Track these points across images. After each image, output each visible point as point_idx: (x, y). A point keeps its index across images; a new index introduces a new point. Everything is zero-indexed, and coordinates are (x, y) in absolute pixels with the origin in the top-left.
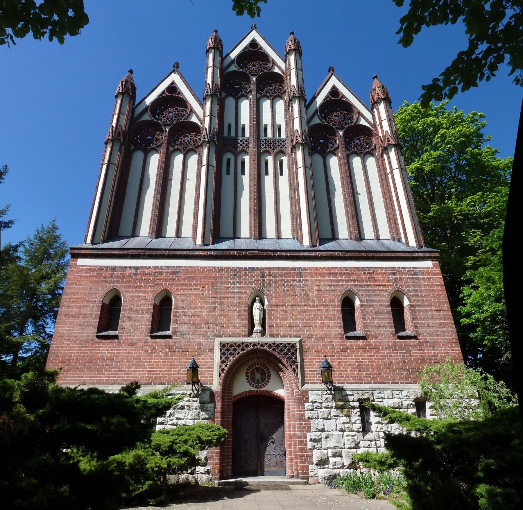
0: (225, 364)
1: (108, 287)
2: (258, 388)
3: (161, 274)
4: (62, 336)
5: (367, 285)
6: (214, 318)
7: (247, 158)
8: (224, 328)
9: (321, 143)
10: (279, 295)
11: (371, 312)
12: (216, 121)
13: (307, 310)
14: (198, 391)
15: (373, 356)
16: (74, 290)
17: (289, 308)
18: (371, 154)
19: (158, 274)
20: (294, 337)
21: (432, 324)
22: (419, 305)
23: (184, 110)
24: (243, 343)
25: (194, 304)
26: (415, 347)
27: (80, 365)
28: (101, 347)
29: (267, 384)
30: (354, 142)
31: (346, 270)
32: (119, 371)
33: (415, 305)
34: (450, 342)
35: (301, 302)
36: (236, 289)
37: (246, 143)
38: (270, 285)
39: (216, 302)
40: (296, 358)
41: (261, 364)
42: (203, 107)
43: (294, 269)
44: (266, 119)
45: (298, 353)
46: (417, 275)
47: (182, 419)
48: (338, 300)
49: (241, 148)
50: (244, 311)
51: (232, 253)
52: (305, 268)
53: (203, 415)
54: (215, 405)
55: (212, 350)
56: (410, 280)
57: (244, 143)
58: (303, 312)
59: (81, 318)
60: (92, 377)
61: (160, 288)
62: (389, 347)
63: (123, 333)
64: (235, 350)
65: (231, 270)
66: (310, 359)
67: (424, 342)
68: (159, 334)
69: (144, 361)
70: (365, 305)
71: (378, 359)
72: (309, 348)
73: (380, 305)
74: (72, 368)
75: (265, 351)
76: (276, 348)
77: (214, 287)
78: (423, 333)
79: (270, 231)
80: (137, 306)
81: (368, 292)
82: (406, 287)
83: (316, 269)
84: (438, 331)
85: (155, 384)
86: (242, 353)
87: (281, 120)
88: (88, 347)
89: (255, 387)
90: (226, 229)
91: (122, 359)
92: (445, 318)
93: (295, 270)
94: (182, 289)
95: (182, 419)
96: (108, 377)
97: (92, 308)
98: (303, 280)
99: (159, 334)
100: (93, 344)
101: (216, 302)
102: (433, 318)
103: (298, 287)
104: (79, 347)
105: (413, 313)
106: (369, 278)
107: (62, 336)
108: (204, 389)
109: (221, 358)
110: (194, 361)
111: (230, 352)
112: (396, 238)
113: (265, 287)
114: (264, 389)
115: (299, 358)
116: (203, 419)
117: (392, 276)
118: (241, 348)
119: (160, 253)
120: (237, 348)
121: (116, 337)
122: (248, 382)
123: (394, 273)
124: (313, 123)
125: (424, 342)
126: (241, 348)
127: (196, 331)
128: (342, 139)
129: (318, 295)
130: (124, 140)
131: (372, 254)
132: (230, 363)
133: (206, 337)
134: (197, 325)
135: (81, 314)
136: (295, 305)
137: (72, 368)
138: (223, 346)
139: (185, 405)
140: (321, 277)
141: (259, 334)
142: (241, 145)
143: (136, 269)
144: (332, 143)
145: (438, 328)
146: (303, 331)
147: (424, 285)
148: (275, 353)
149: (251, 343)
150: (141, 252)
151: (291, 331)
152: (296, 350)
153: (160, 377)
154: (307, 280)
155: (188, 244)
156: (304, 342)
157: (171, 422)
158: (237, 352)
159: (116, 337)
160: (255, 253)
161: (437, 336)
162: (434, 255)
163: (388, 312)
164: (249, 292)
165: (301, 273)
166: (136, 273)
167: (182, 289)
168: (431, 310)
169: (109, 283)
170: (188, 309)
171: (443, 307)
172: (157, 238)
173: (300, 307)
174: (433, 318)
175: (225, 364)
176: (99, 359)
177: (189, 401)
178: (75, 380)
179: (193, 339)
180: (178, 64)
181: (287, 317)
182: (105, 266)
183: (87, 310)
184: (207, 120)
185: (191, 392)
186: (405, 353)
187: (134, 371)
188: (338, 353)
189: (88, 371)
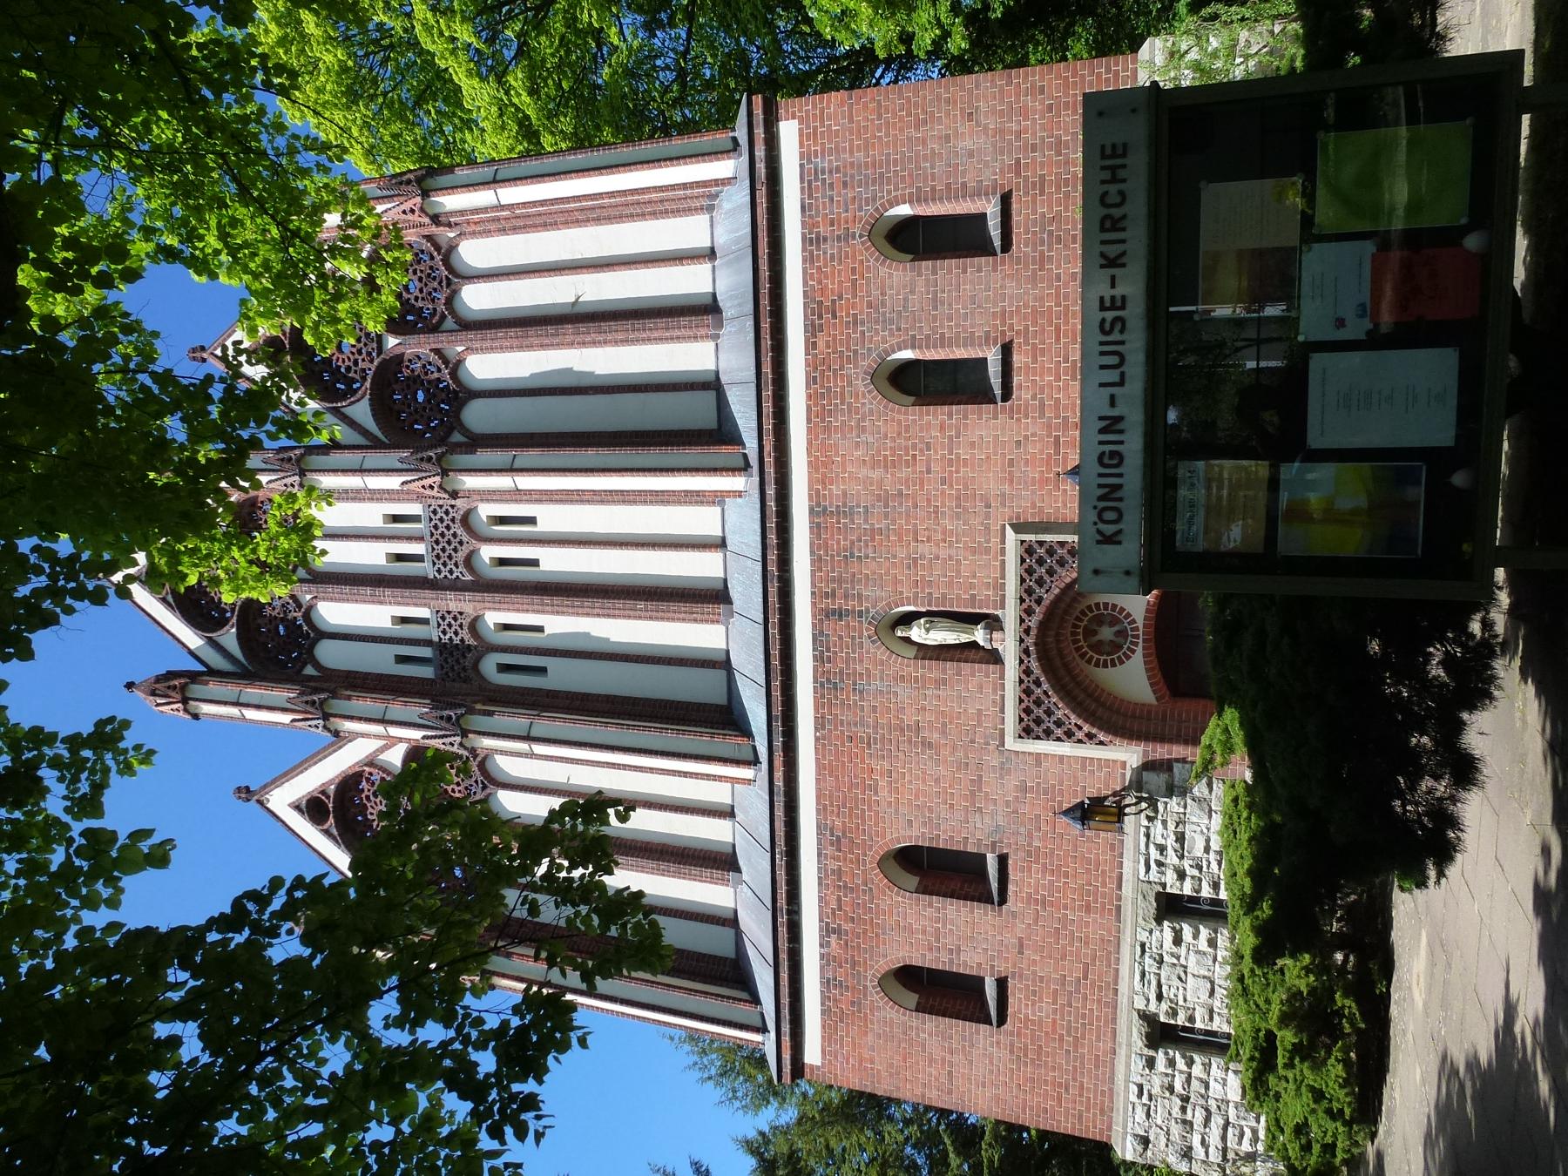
0: (1074, 729)
1: (875, 996)
2: (1137, 637)
3: (839, 873)
4: (997, 1099)
5: (855, 323)
6: (954, 748)
7: (493, 618)
8: (980, 723)
9: (427, 400)
10: (888, 574)
11: (935, 320)
12: (397, 709)
13: (929, 501)
14: (1140, 800)
15: (1058, 329)
16: (884, 1074)
17: (924, 549)
18: (448, 253)
19: (840, 879)
20: (1003, 542)
21: (967, 144)
22: (910, 175)
23: (368, 780)
24: (1021, 681)
25: (917, 796)
26: (1034, 202)
27: (1068, 1063)
28: (1026, 1016)
29: (1129, 615)
30: (416, 299)
31: (815, 383)
32: (1086, 978)
33: (911, 186)
34: (1018, 95)
35: (908, 515)
36: (873, 687)
37: (449, 619)
38: (860, 596)
39: (910, 741)
40: (1062, 544)
41: (1075, 626)
42: (355, 736)
43: (816, 529)
44: (372, 556)
45: (1048, 538)
46: (823, 173)
47: (1208, 841)
48: (899, 412)
49: (465, 634)
50: (934, 670)
51: (777, 694)
52: (810, 496)
53: (1200, 789)
54: (1177, 760)
55: (1038, 757)
56: (839, 195)
57: (450, 625)
58: (936, 512)
59: (955, 1059)
60: (1098, 1038)
61: (877, 876)
62: (1034, 279)
63: (992, 967)
64: (1038, 703)
65: (823, 696)
66: (1065, 506)
67: (1018, 174)
68: (994, 885)
69: (1064, 920)
70: (914, 337)
71: (1066, 315)
72: (1034, 506)
73: (912, 292)
74: (1075, 1080)
75: (1043, 626)
76: (1035, 596)
77: (869, 744)
78: (993, 172)
79: (690, 281)
80: (924, 932)
81: (877, 322)
82: (861, 209)
83: (813, 465)
84: (986, 128)
85: (1119, 898)
86: (1045, 686)
87: (371, 515)
88: (1026, 1046)
89: (1136, 644)
90: (695, 411)
91: (1056, 971)
92: (948, 101)
93: (819, 525)
94: (876, 825)
95: (1208, 841)
96: (1099, 1001)
97: (930, 1035)
98: (845, 505)
99: (994, 885)
100: (1019, 1034)
101: (910, 741)
102: (948, 138)
103: (866, 521)
104: (1026, 1064)
105: (934, 197)
106: (834, 317)
107: (997, 1099)
108: (1137, 784)
109: (1059, 739)
110: (1066, 813)
111: (1044, 716)
112: (705, 202)
113: (868, 611)
114: (1140, 623)
115: (1062, 538)
116: (1211, 790)
117: (830, 249)
118: (1033, 687)
119: (782, 874)
120: (1033, 697)
121: (1002, 984)
122: (1122, 662)
123: (818, 239)
124: (370, 423)
125: (1018, 174)
126: (1033, 687)
127: (987, 794)
128: (413, 339)
129: (886, 467)
130: (460, 706)
131: (765, 302)
132: (1073, 717)
133: (1003, 770)
134: (973, 793)
135: (943, 1060)
136: (916, 533)
137: (1075, 1080)
138: (1026, 732)
139: (1175, 833)
140: (837, 454)
141: (996, 635)
142: (456, 633)
143: (827, 931)
144: (424, 366)
145: (978, 124)
146: (988, 516)
147: (851, 152)
148: (1048, 598)
149: (1021, 661)
150: (783, 919)
151: (988, 551)
152: (1041, 543)
153: (1104, 885)
154: (845, 494)
155: (754, 803)
156: (1018, 518)
157: (1214, 866)
158: (1043, 697)
159: (1002, 984)
160: (774, 631)
161: (1002, 131)
162: (758, 111)
163: (935, 272)
164: (882, 654)
165: (825, 509)
166: (838, 931)
167: (876, 825)
168: (924, 142)
169: (865, 995)
170: (930, 810)
171: (916, 103)
172: (738, 870)
173: (923, 521)
174: (948, 138)
175: (1074, 729)
176: (1054, 1021)
177: (1164, 822)
178: (1104, 1074)
179: (1008, 804)
180: (239, 790)
181: (950, 558)
182: (823, 1004)
183: (934, 1046)
184: (395, 731)
185: (1143, 815)
186: (1051, 233)
187: (1087, 943)
188: (1049, 426)
189: (1083, 1046)
